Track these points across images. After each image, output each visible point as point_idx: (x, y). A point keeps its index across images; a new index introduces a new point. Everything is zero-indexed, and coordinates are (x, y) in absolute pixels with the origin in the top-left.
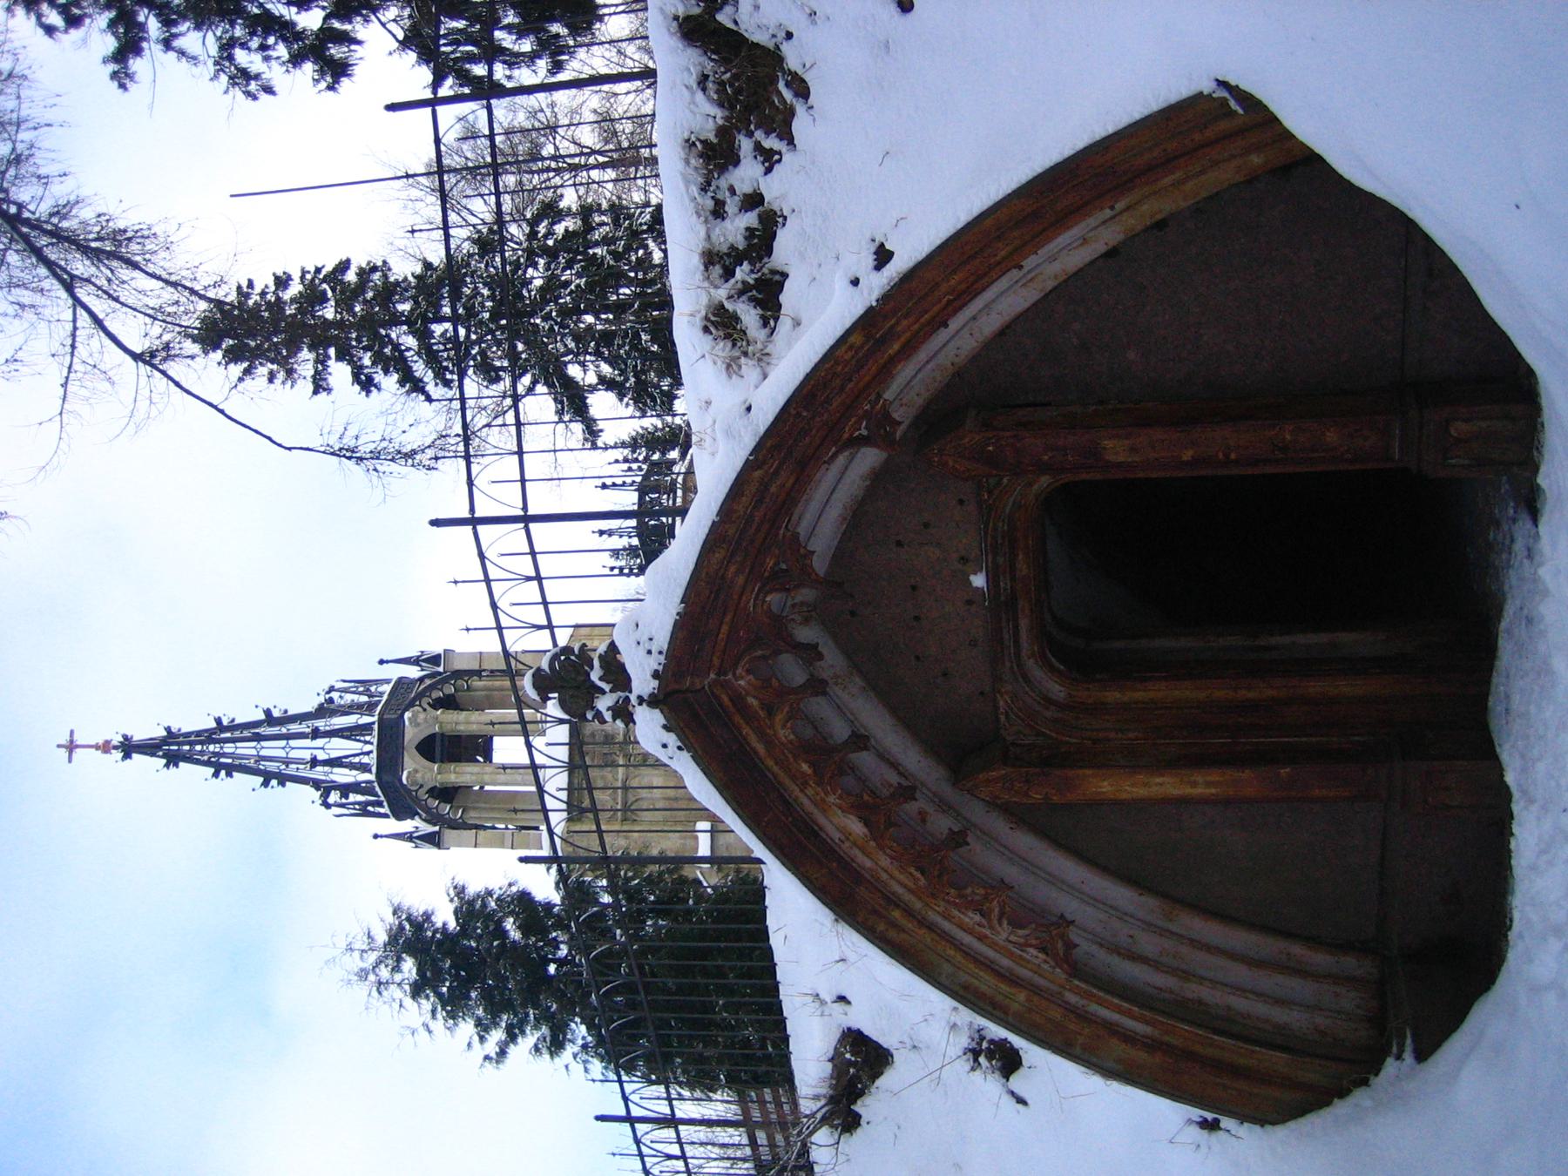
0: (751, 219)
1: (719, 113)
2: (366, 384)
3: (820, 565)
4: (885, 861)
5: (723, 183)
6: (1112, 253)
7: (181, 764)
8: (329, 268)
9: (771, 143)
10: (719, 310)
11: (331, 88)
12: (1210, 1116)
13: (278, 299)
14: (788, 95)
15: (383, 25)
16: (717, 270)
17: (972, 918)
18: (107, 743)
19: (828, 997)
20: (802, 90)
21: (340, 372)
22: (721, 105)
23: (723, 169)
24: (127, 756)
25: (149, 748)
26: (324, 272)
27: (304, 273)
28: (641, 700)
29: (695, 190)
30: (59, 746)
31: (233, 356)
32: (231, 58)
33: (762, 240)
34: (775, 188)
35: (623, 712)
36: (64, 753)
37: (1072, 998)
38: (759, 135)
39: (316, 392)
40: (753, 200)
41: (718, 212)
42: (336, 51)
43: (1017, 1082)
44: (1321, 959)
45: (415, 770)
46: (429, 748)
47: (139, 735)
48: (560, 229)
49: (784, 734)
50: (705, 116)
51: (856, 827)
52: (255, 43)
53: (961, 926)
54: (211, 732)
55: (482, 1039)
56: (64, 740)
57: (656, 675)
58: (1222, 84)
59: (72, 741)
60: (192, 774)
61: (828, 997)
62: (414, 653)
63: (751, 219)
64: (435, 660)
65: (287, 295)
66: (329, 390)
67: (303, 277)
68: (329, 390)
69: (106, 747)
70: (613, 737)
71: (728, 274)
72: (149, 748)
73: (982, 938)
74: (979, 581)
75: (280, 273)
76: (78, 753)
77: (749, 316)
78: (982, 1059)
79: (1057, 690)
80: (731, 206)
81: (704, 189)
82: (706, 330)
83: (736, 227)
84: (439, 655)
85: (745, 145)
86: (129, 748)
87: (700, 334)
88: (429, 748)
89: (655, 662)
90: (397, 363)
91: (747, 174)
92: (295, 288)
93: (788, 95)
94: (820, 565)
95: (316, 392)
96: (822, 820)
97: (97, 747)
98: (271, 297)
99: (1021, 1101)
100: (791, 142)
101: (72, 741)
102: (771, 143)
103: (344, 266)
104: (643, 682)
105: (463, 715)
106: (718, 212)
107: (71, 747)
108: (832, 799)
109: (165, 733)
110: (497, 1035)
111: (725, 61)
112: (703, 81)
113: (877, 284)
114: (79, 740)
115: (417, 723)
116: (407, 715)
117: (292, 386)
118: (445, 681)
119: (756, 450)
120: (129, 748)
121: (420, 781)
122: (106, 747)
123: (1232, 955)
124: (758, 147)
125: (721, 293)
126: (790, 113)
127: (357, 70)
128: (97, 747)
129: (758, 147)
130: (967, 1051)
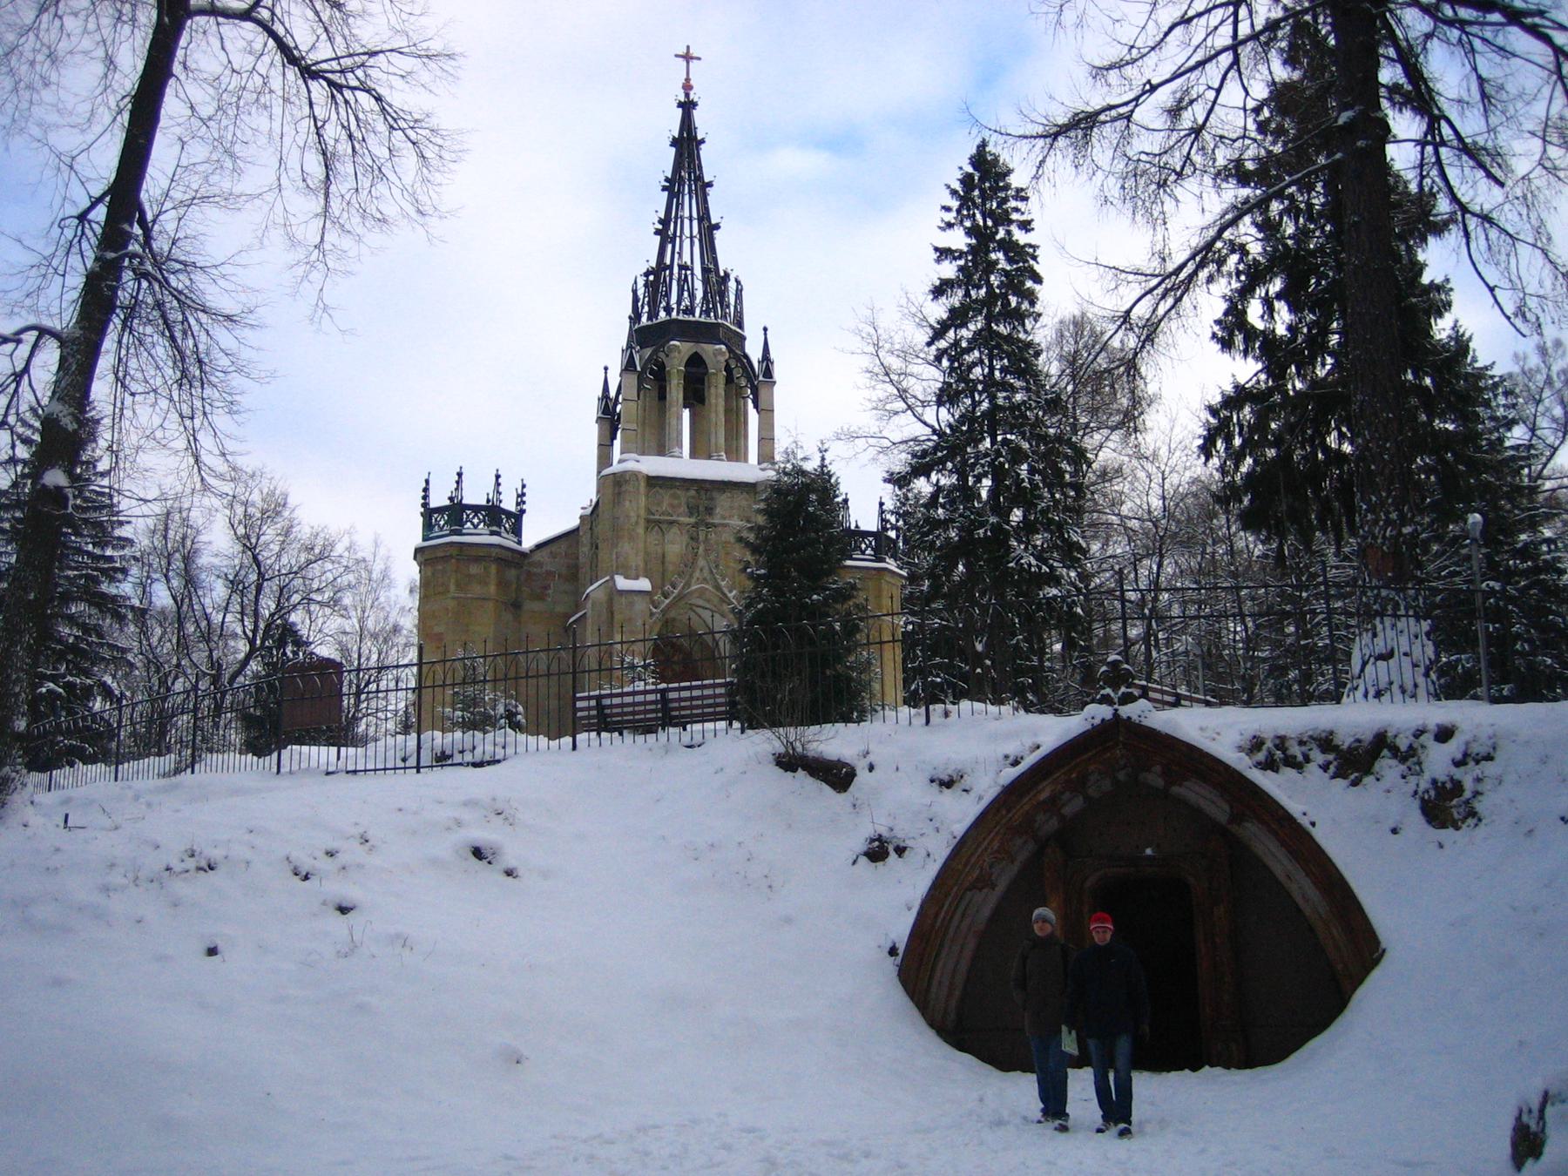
0: (1300, 758)
1: (1345, 747)
2: (939, 291)
3: (1175, 789)
4: (1026, 808)
5: (1314, 746)
6: (1299, 910)
7: (674, 149)
8: (1037, 268)
9: (1332, 769)
10: (1262, 743)
11: (1214, 336)
12: (901, 951)
13: (1011, 222)
14: (1352, 777)
15: (1256, 375)
16: (1277, 742)
17: (996, 845)
18: (691, 88)
19: (871, 758)
20: (1355, 783)
21: (949, 270)
22: (1349, 747)
23: (1320, 746)
24: (680, 105)
25: (687, 123)
26: (1032, 262)
27: (1034, 247)
28: (1116, 710)
29: (1310, 733)
30: (688, 47)
31: (967, 181)
32: (1233, 251)
33: (1291, 762)
34: (1312, 768)
35: (1106, 700)
36: (682, 51)
37: (955, 889)
38: (1335, 763)
39: (936, 249)
40: (1307, 759)
41: (1301, 743)
42: (1239, 339)
43: (864, 860)
44: (953, 1003)
45: (681, 349)
46: (696, 362)
47: (697, 114)
48: (1065, 466)
49: (1092, 768)
50: (1344, 740)
51: (1044, 796)
52: (1241, 267)
53: (993, 840)
54: (700, 178)
55: (751, 529)
56: (694, 53)
57: (1129, 718)
58: (1384, 951)
59: (692, 58)
60: (666, 158)
61: (871, 758)
62: (773, 355)
63: (1300, 758)
64: (768, 373)
65: (1014, 228)
66: (938, 261)
67: (1031, 246)
68: (938, 261)
69: (687, 87)
70: (710, 514)
71: (1277, 747)
72: (687, 123)
73: (986, 849)
74: (1149, 851)
75: (1033, 225)
76: (683, 63)
77: (1261, 756)
78: (877, 843)
79: (1088, 884)
80: (1304, 749)
81: (1311, 737)
82: (1254, 737)
83: (1296, 750)
84: (771, 377)
85: (1330, 757)
86: (687, 107)
87: (1253, 733)
88: (696, 362)
89: (1135, 718)
90: (957, 317)
91: (1318, 757)
92: (1020, 237)
93: (1352, 777)
94: (1175, 789)
95: (936, 249)
96: (1050, 780)
97: (688, 80)
98: (1015, 216)
99: (854, 862)
100: (1333, 777)
101: (692, 58)
102: (1332, 769)
103: (1038, 279)
104: (1126, 711)
105: (722, 391)
106: (1301, 743)
107: (688, 57)
108: (1059, 787)
109: (699, 138)
110: (751, 537)
111: (1367, 752)
112: (1359, 741)
113: (1304, 822)
114: (693, 64)
115: (715, 353)
116: (723, 347)
117: (940, 228)
118: (750, 380)
119: (1235, 771)
120: (687, 107)
121: (672, 355)
122: (687, 87)
123: (958, 962)
124: (1330, 763)
125: (1269, 744)
126: (1345, 777)
127: (1226, 356)
128: (688, 80)
129: (1330, 763)
130: (880, 836)
